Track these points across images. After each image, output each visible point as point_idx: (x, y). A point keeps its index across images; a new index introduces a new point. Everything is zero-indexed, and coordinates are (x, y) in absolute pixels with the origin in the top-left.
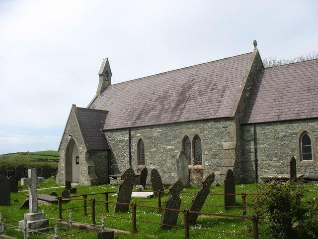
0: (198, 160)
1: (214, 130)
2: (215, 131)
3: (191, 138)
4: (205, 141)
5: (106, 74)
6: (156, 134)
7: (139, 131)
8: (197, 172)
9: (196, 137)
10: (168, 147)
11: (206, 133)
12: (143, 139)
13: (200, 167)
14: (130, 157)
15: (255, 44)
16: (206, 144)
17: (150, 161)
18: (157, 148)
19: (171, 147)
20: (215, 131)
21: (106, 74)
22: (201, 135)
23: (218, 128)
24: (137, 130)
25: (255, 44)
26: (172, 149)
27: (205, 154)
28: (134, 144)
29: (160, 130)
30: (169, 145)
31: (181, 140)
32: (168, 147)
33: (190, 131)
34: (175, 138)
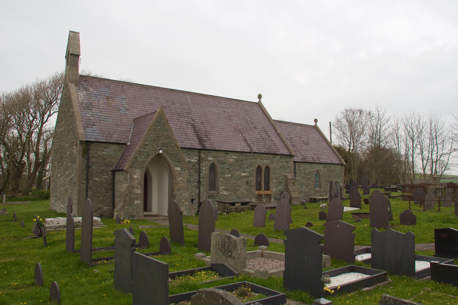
0: (267, 187)
1: (280, 164)
2: (281, 164)
3: (263, 168)
4: (274, 171)
5: (73, 57)
6: (231, 160)
7: (211, 154)
8: (266, 196)
9: (267, 168)
10: (243, 174)
11: (275, 165)
12: (216, 163)
13: (269, 192)
14: (199, 182)
15: (260, 97)
16: (274, 174)
17: (224, 187)
18: (232, 174)
19: (246, 174)
20: (281, 164)
21: (73, 57)
22: (271, 166)
23: (282, 162)
24: (208, 153)
25: (260, 97)
26: (247, 176)
27: (273, 182)
28: (205, 168)
29: (236, 157)
30: (244, 172)
31: (254, 168)
32: (243, 174)
33: (264, 162)
34: (250, 166)
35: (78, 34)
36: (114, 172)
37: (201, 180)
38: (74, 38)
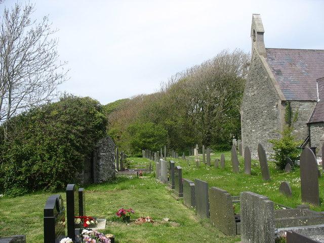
35: (255, 16)
36: (309, 125)
37: (311, 135)
38: (255, 21)
